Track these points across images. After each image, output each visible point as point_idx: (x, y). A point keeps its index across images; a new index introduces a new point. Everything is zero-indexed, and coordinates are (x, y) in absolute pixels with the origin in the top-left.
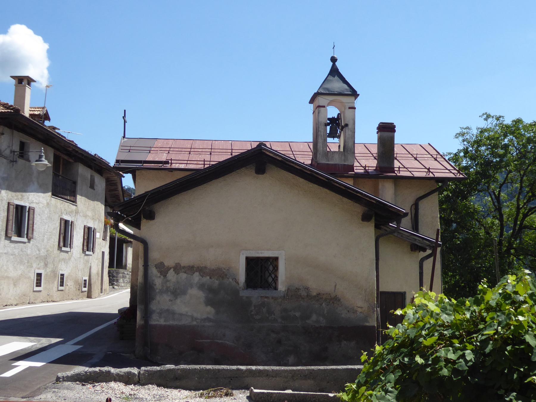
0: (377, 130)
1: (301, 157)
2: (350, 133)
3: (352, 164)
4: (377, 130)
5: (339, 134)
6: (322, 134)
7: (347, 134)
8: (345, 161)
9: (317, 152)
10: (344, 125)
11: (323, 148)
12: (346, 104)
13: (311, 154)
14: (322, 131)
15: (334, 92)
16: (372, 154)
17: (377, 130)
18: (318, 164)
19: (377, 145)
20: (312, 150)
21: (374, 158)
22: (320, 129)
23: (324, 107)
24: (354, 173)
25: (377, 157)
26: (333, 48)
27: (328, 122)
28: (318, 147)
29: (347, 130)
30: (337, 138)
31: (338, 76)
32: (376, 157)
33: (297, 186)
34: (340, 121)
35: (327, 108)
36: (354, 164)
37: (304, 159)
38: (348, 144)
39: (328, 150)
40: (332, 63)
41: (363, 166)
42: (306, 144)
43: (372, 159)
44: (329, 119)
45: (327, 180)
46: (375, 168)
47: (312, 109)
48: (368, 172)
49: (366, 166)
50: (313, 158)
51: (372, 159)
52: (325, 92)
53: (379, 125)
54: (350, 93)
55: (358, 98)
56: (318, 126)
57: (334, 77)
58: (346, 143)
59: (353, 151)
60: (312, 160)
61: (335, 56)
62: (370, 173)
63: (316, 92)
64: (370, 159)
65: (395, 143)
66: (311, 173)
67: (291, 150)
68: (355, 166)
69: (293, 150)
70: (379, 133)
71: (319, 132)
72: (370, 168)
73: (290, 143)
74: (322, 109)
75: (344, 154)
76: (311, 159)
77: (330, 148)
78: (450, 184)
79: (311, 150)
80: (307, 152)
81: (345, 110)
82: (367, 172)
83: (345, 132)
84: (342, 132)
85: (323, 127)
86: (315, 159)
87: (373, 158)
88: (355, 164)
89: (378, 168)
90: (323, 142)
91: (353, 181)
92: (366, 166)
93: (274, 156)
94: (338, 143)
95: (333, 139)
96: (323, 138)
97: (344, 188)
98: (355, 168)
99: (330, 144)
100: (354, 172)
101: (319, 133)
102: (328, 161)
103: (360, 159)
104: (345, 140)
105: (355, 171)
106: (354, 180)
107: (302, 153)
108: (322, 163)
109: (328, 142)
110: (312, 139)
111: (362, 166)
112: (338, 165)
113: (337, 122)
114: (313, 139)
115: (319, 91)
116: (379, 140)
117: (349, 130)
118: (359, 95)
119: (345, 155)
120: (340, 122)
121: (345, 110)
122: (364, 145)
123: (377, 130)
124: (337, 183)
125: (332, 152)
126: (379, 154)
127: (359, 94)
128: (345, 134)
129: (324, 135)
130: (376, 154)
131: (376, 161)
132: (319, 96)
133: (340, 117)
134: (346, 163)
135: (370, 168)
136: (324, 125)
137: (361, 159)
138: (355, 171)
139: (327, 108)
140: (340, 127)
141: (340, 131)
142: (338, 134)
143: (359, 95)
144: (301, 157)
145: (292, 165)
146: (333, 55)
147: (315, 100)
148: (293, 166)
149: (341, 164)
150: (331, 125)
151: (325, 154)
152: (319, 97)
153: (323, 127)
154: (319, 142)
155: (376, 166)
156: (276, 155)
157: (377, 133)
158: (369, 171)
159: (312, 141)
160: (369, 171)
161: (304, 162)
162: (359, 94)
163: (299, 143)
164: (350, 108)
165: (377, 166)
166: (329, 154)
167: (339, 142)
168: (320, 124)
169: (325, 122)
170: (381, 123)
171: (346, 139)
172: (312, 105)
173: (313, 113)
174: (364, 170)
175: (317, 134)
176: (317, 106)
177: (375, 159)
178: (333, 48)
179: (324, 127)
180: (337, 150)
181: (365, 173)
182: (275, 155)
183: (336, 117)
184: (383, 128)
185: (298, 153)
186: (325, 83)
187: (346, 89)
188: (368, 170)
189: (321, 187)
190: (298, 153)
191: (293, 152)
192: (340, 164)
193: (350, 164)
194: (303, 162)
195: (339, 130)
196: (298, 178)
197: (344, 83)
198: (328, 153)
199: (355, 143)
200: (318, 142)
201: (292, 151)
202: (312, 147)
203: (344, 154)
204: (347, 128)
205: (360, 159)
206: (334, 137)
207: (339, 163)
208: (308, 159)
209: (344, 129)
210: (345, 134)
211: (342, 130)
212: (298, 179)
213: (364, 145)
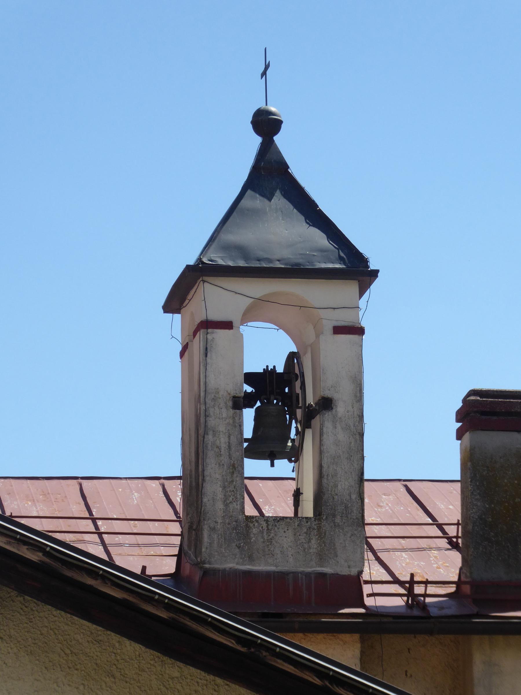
0: (460, 424)
1: (131, 545)
2: (342, 436)
3: (354, 572)
4: (458, 421)
5: (297, 444)
6: (223, 441)
7: (329, 440)
8: (322, 558)
9: (199, 522)
10: (316, 404)
11: (226, 505)
12: (322, 313)
13: (176, 528)
14: (222, 428)
15: (270, 261)
16: (440, 527)
17: (458, 421)
18: (206, 572)
19: (459, 485)
20: (180, 508)
21: (450, 543)
22: (212, 422)
23: (228, 325)
24: (362, 611)
25: (460, 541)
26: (264, 74)
27: (249, 389)
28: (205, 500)
29: (328, 426)
30: (286, 460)
31: (286, 196)
32: (457, 537)
33: (113, 676)
34: (298, 384)
35: (244, 329)
36: (361, 572)
37: (145, 551)
38: (336, 486)
39: (250, 511)
40: (258, 140)
41: (402, 579)
42: (155, 484)
43: (439, 549)
44: (250, 378)
45: (243, 646)
46: (452, 589)
47: (178, 333)
48: (424, 607)
49: (416, 579)
50: (186, 547)
51: (439, 549)
52: (231, 264)
53: (465, 401)
54: (338, 266)
55: (372, 287)
56: (203, 408)
57: (270, 199)
58: (325, 481)
59: (355, 513)
60: (179, 556)
61: (273, 109)
62: (434, 612)
63: (192, 262)
64: (431, 549)
65: (180, 475)
66: (172, 615)
67: (87, 516)
68: (366, 582)
69: (95, 514)
70: (467, 436)
71: (211, 433)
72: (432, 590)
73: (85, 483)
74: (220, 334)
75: (319, 528)
76: (176, 551)
77: (260, 501)
78: (504, 543)
79: (176, 513)
80: (156, 524)
81: (318, 336)
82: (418, 603)
83: (321, 434)
84: (309, 434)
85: (224, 410)
86: (191, 553)
87: (443, 543)
88: (366, 570)
89: (467, 589)
90: (229, 478)
91: (359, 645)
92: (416, 579)
93: (9, 543)
94: (293, 479)
95: (268, 462)
96: (225, 459)
97: (317, 681)
98: (367, 589)
99: (260, 483)
100: (363, 606)
101: (210, 438)
102: (251, 559)
103: (387, 550)
104: (321, 467)
105: (369, 602)
106: (362, 641)
107: (135, 526)
108: (224, 570)
109: (246, 475)
110: (180, 463)
111: (396, 581)
112: (295, 574)
113: (287, 390)
114: (183, 465)
115: (205, 260)
116: (469, 464)
117: (338, 425)
118: (375, 274)
119: (321, 535)
120: (298, 390)
121: (318, 336)
122: (407, 487)
123: (460, 424)
124: (285, 661)
125: (267, 520)
126: (470, 527)
127: (377, 271)
128: (321, 441)
129: (229, 447)
130: (458, 524)
131: (456, 558)
132: (204, 281)
133: (297, 371)
134: (327, 570)
135: (432, 590)
136: (230, 404)
137: (395, 550)
138: (369, 602)
139: (244, 329)
140: (299, 413)
141: (297, 428)
142: (290, 444)
143: (375, 274)
144: (131, 545)
145: (90, 581)
146: (262, 105)
147: (189, 297)
148: (91, 589)
149: (308, 575)
150: (258, 404)
151: (235, 528)
152: (206, 284)
153: (227, 412)
154: (207, 478)
155: (456, 579)
156: (19, 540)
157: (460, 435)
158: (428, 600)
159: (459, 479)
160: (428, 600)
161: (144, 568)
162: (377, 271)
163: (124, 481)
164: (338, 330)
165: (463, 579)
166: (255, 531)
167: (293, 475)
168: (214, 399)
169: (233, 393)
170: (473, 392)
171: (325, 466)
172: (177, 317)
173: (182, 354)
174: (407, 595)
175: (201, 438)
176: (198, 321)
177: (454, 546)
178: (264, 74)
179: (231, 411)
180: (289, 512)
181: (409, 612)
182: (15, 539)
183: (280, 369)
184: (483, 413)
185: (118, 526)
186: (231, 219)
187: (322, 250)
188: (425, 595)
189: (217, 678)
190: (118, 526)
191: (100, 523)
192: (302, 573)
193: (344, 571)
194: (138, 571)
195: (294, 425)
196: (115, 638)
197: (314, 226)
198: (247, 526)
199: (366, 477)
200: (203, 480)
201: (94, 520)
202: (178, 498)
203: (319, 528)
204: (327, 415)
205: (387, 550)
206: (272, 457)
207: (294, 569)
208: (164, 551)
209: (316, 422)
210: (321, 441)
211: (306, 423)
212: (117, 645)
213: (407, 487)
